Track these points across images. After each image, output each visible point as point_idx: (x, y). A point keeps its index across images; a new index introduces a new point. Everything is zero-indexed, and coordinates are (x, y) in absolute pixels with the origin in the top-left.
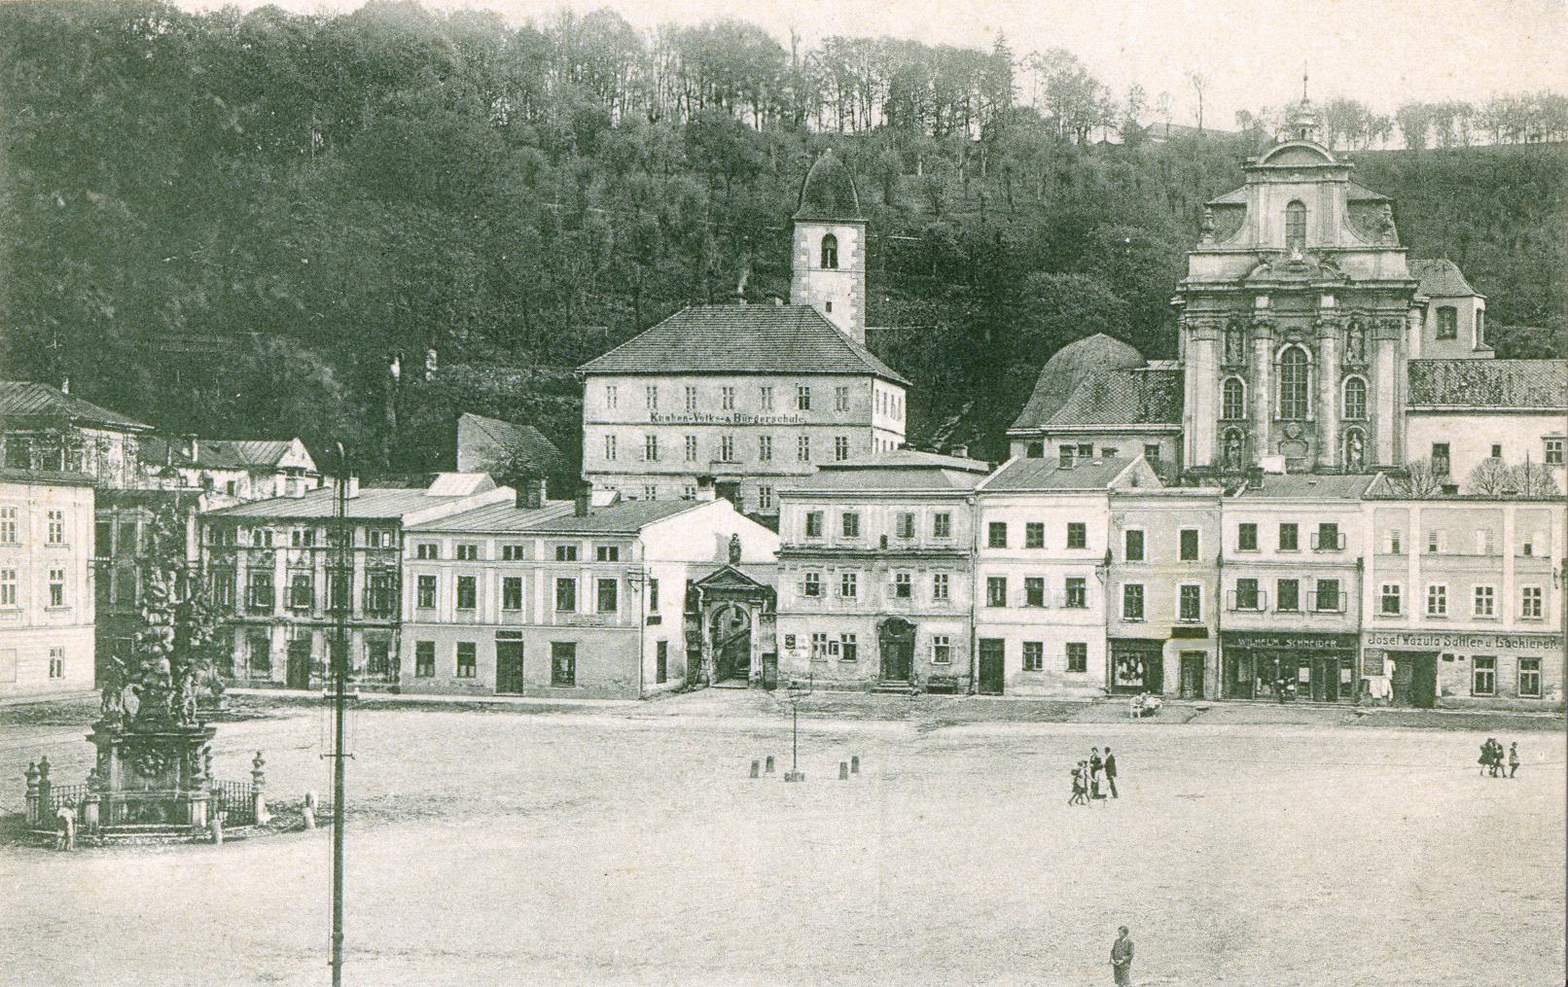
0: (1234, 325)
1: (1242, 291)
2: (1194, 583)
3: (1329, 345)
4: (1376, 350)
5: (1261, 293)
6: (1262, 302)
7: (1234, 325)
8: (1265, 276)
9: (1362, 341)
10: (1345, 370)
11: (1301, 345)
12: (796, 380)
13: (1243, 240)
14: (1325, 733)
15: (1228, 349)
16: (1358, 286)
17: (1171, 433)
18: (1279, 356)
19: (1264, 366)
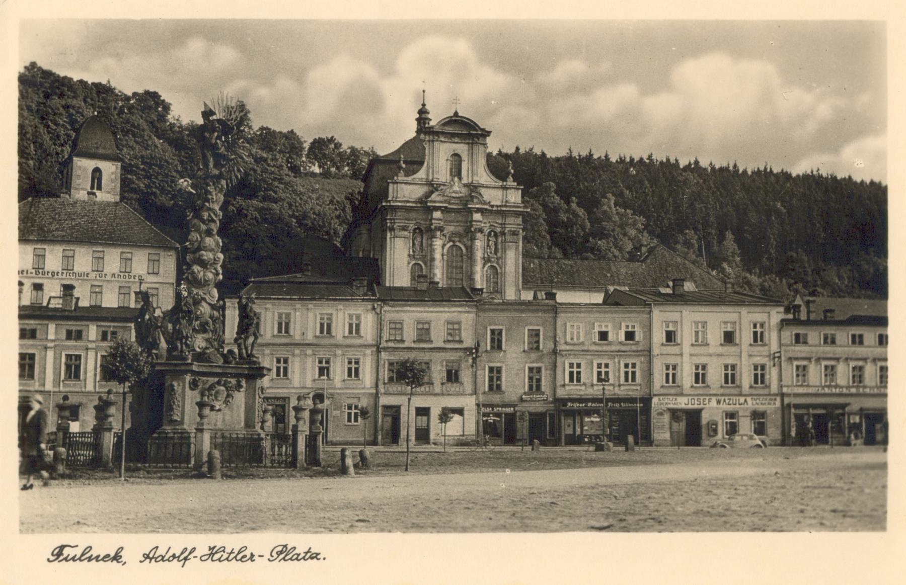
0: (418, 231)
1: (424, 206)
2: (30, 351)
3: (479, 244)
4: (504, 250)
5: (436, 209)
6: (437, 215)
7: (418, 231)
8: (438, 199)
9: (496, 244)
10: (486, 260)
11: (458, 244)
12: (293, 342)
13: (421, 174)
14: (497, 449)
15: (414, 244)
16: (495, 209)
17: (376, 437)
18: (445, 251)
19: (438, 256)
